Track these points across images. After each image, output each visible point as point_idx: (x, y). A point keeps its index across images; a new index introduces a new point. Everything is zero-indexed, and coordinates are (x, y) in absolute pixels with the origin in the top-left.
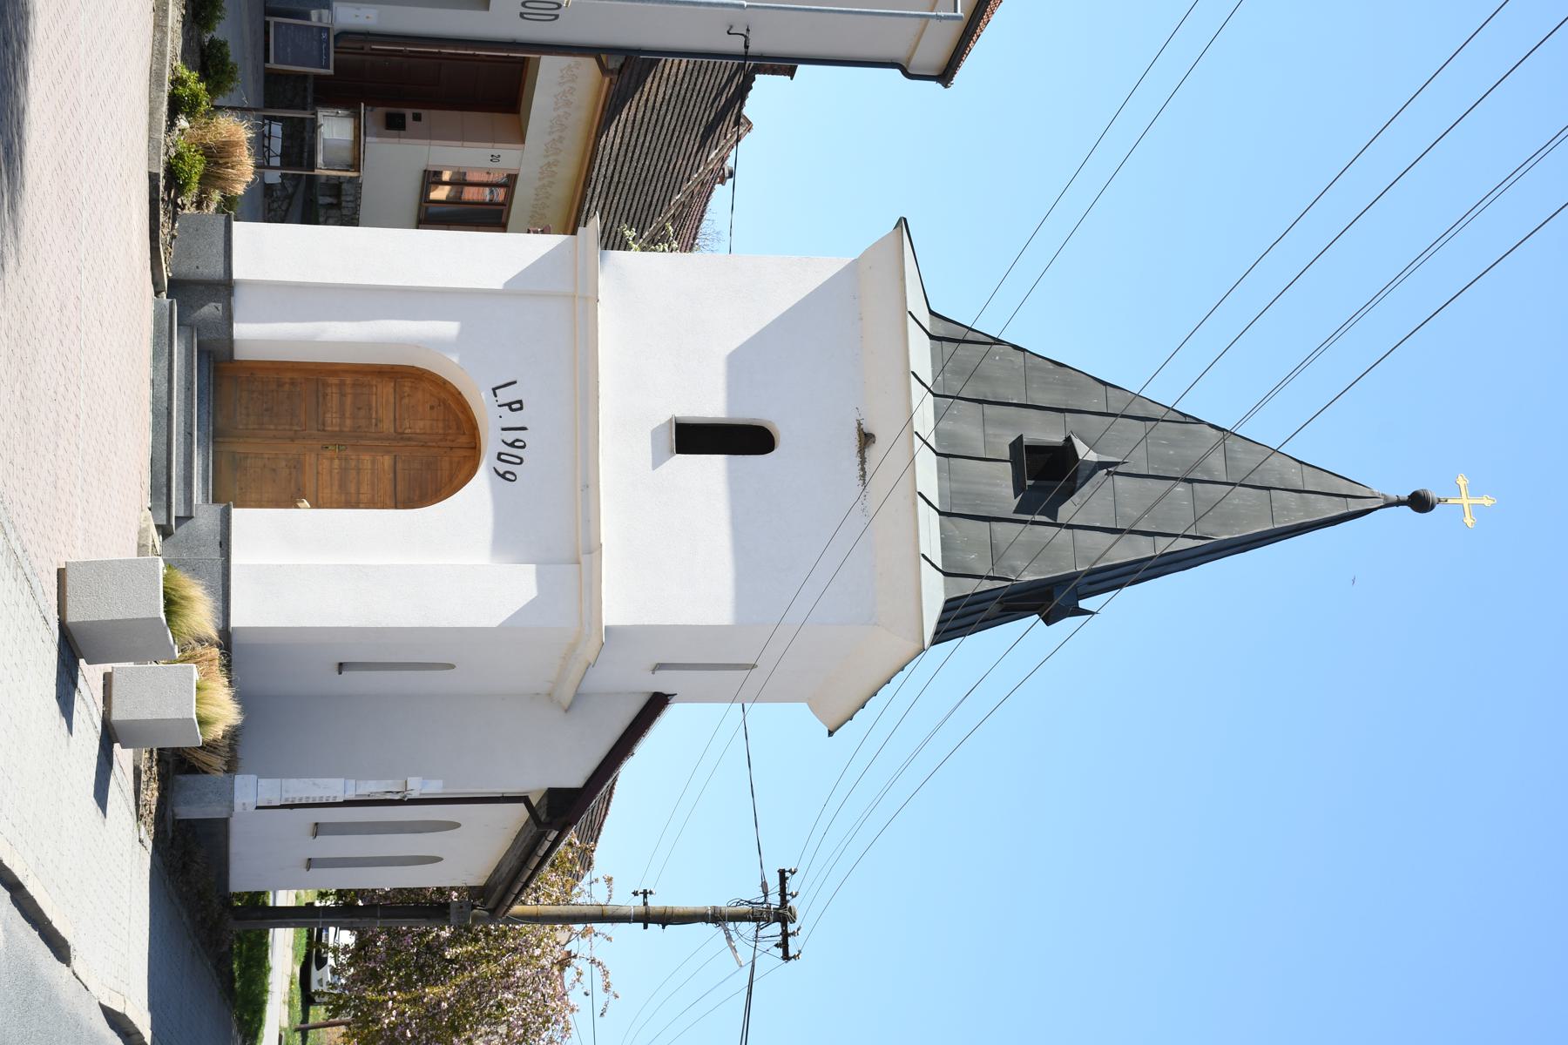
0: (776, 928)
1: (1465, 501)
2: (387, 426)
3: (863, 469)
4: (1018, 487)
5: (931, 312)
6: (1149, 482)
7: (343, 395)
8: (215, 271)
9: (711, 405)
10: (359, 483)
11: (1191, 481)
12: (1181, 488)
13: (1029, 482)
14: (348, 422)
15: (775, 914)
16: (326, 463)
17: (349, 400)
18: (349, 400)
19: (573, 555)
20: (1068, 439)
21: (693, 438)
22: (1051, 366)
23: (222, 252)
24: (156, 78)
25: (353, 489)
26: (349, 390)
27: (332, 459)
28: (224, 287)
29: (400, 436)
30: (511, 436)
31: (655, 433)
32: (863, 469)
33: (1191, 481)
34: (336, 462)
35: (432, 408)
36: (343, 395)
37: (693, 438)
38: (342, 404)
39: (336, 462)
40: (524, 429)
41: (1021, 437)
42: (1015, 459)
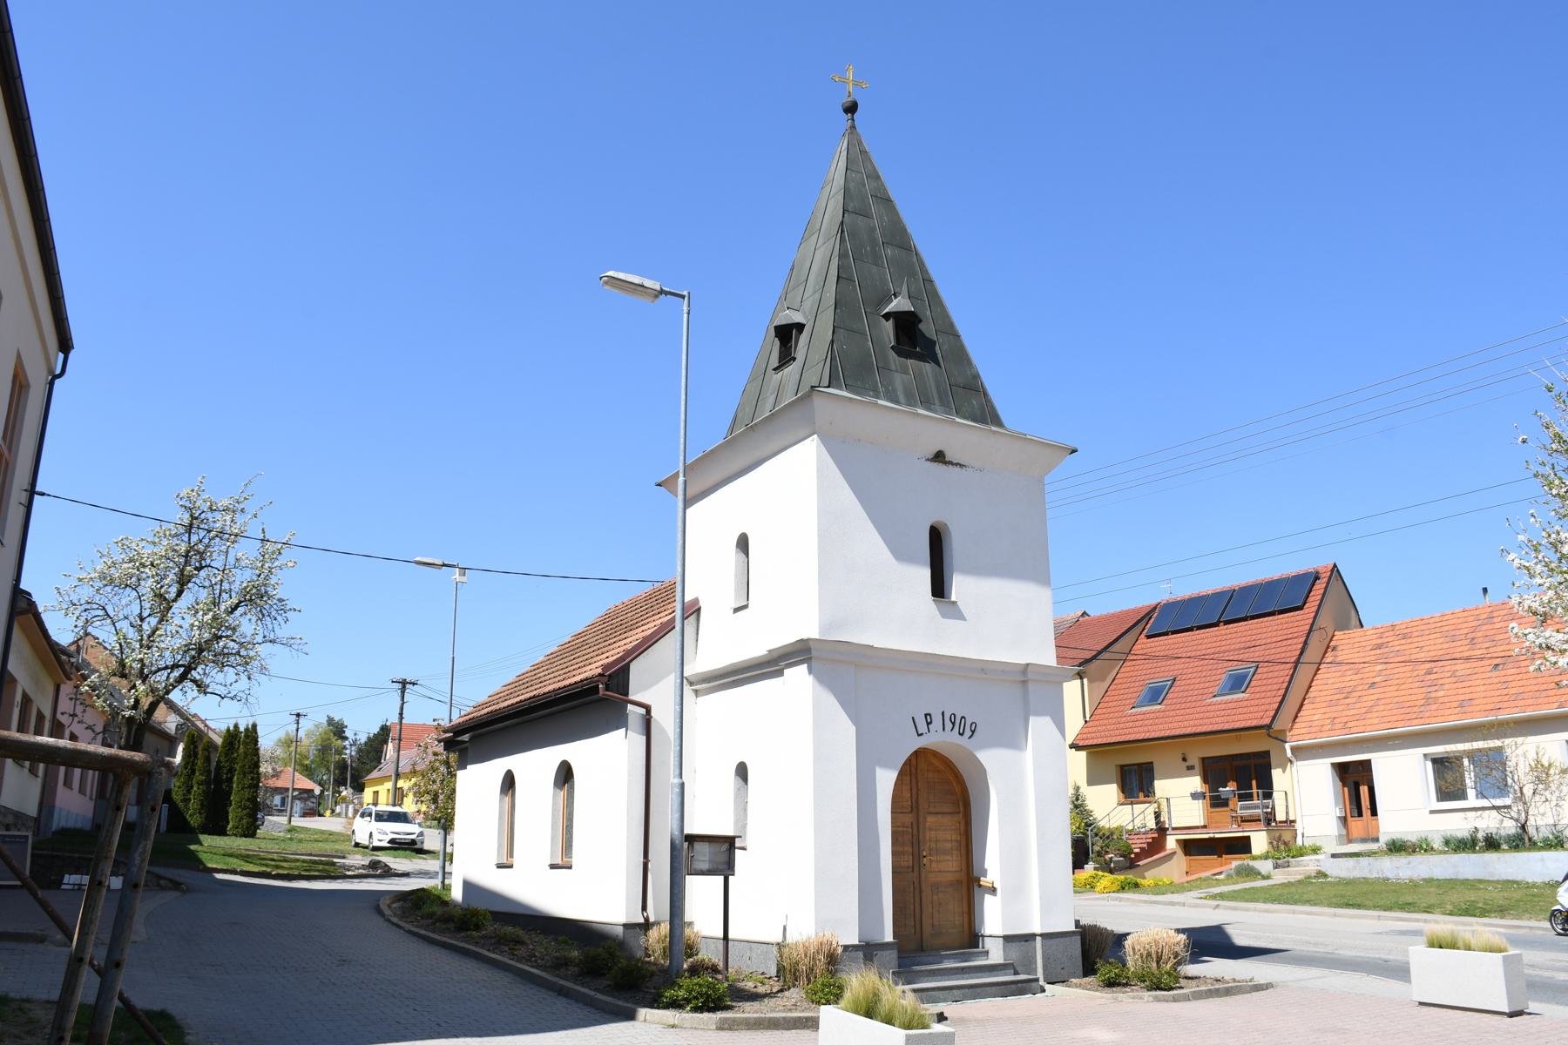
1: (850, 91)
19: (1025, 688)
30: (949, 725)
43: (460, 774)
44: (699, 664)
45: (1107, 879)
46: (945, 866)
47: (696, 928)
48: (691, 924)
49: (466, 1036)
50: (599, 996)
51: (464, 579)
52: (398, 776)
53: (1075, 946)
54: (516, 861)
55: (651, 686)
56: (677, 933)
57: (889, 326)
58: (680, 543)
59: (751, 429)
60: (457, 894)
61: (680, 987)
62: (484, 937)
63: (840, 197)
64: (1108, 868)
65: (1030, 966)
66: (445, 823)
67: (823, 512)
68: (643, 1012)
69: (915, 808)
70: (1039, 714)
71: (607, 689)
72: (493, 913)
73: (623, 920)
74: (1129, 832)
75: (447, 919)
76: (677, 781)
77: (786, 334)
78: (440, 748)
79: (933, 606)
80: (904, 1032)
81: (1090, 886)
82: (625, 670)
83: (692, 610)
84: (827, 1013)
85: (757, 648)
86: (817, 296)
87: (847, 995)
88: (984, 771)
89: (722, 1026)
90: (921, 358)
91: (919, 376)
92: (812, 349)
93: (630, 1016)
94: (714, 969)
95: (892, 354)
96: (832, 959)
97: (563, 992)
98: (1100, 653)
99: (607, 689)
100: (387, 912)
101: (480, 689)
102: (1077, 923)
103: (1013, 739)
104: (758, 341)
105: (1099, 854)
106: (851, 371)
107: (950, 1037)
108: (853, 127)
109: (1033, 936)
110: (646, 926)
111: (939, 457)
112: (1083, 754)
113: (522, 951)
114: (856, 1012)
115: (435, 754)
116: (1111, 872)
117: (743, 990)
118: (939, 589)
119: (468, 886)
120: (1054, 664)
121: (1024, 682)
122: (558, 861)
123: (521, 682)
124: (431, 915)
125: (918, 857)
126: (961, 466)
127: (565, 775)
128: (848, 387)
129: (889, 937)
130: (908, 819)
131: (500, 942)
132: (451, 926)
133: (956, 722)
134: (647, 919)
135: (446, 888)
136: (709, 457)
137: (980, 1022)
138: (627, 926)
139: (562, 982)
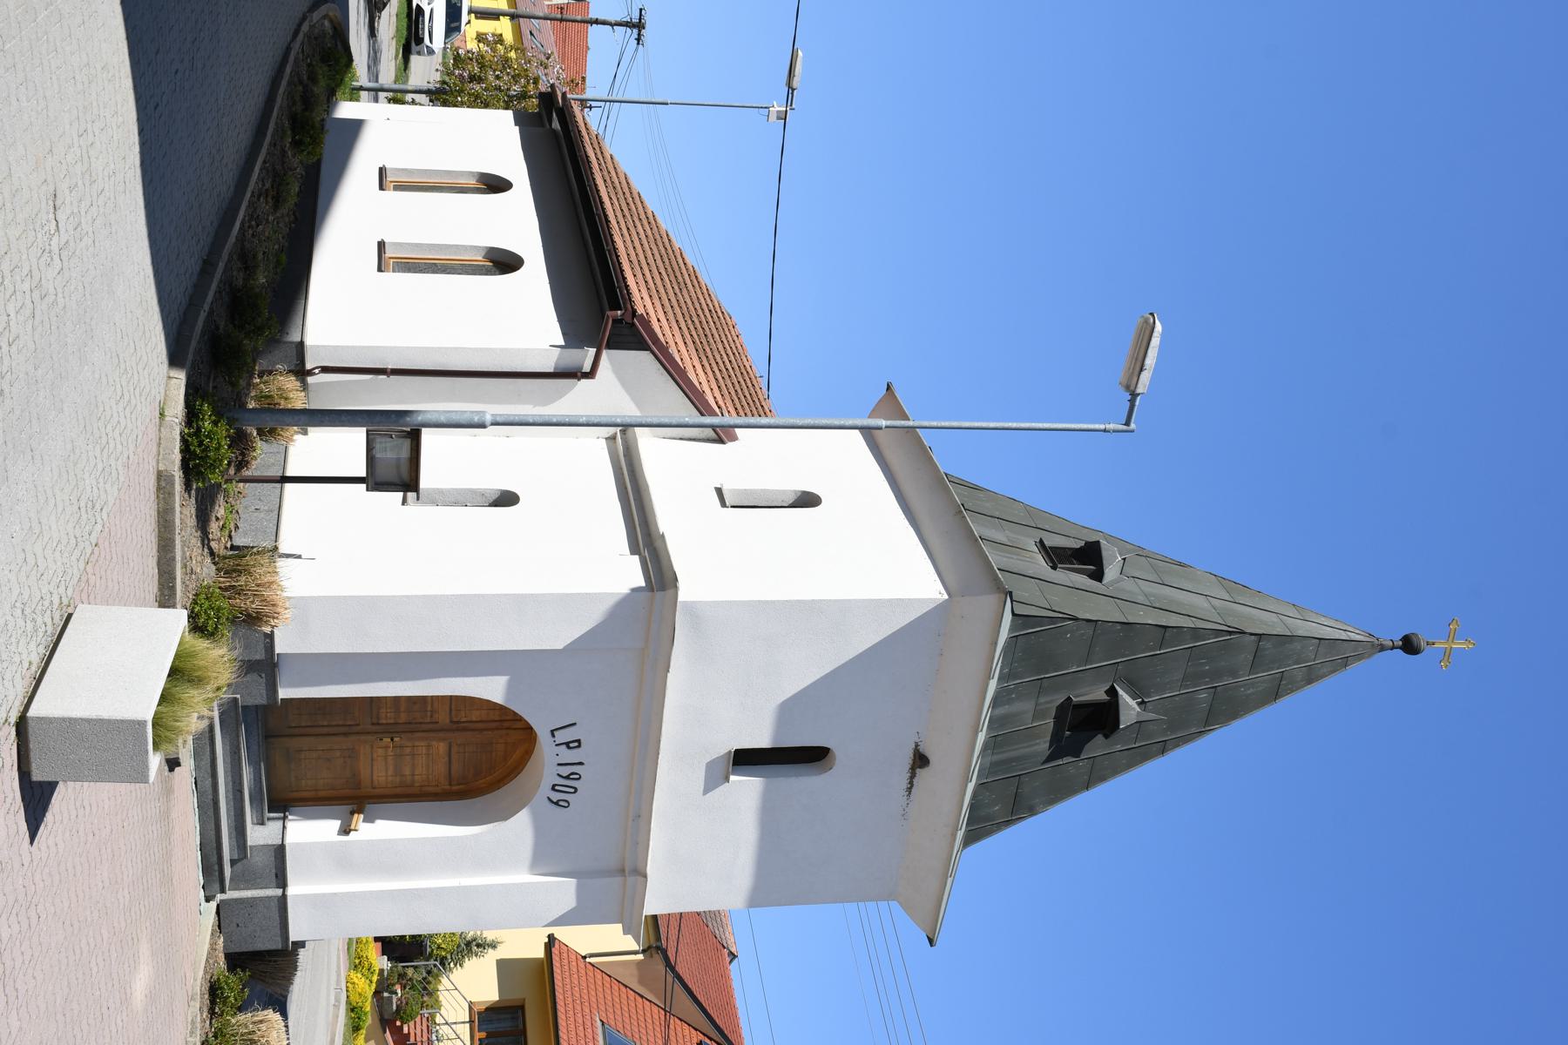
0: (635, 31)
1: (1437, 644)
3: (911, 783)
15: (638, 26)
19: (613, 877)
27: (387, 747)
30: (565, 771)
32: (911, 783)
34: (390, 752)
43: (510, 113)
44: (649, 445)
45: (365, 987)
46: (379, 765)
47: (299, 438)
48: (305, 433)
49: (143, 144)
50: (203, 316)
51: (773, 117)
52: (513, 17)
53: (267, 942)
54: (391, 195)
55: (617, 383)
56: (288, 419)
57: (1098, 694)
58: (799, 422)
59: (959, 511)
60: (346, 110)
61: (215, 423)
62: (284, 152)
63: (1279, 630)
64: (383, 986)
65: (240, 881)
66: (441, 96)
67: (844, 607)
68: (180, 378)
69: (457, 726)
70: (580, 892)
71: (616, 321)
72: (318, 164)
73: (311, 340)
74: (431, 1019)
75: (308, 101)
76: (488, 418)
77: (1088, 557)
78: (543, 88)
79: (723, 751)
80: (149, 717)
81: (358, 964)
82: (640, 345)
83: (721, 435)
84: (178, 619)
85: (667, 520)
86: (1141, 599)
87: (202, 644)
88: (506, 819)
89: (163, 479)
90: (1056, 737)
91: (1030, 734)
92: (1068, 593)
93: (175, 360)
94: (242, 464)
95: (1060, 699)
96: (253, 619)
97: (207, 266)
98: (673, 969)
99: (616, 321)
100: (316, 16)
101: (622, 142)
102: (301, 944)
103: (545, 858)
104: (1083, 515)
105: (402, 976)
106: (1036, 644)
107: (142, 777)
108: (1382, 648)
109: (282, 883)
110: (301, 373)
111: (920, 760)
112: (540, 953)
113: (264, 206)
114: (177, 656)
115: (536, 81)
116: (377, 993)
117: (213, 503)
118: (745, 759)
119: (355, 126)
120: (650, 909)
121: (622, 871)
122: (389, 253)
123: (632, 199)
124: (313, 78)
125: (391, 730)
126: (909, 790)
127: (504, 262)
128: (1013, 641)
129: (283, 693)
130: (443, 717)
131: (277, 176)
132: (299, 107)
133: (569, 781)
134: (311, 373)
135: (354, 95)
136: (923, 453)
137: (166, 816)
138: (301, 345)
139: (221, 265)
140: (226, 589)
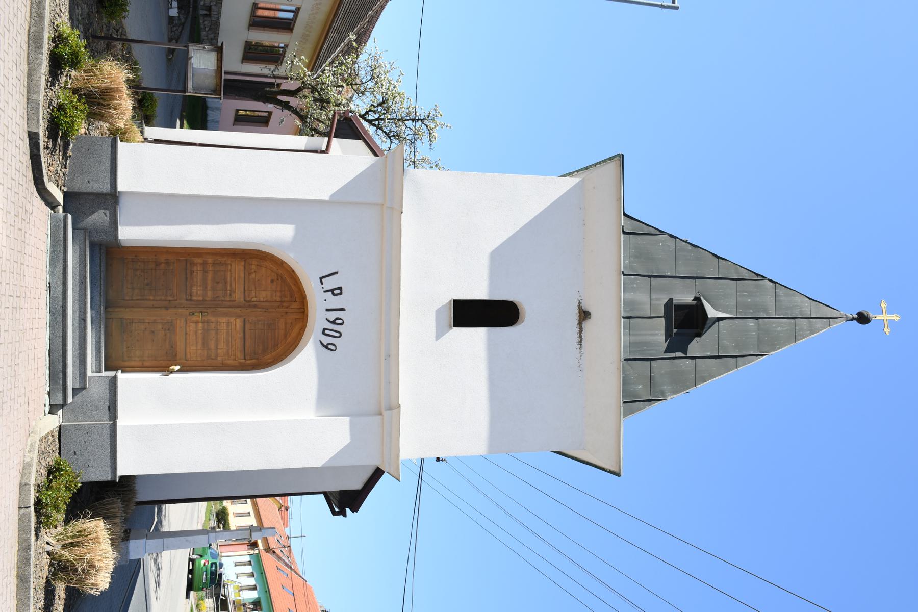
1: (884, 317)
2: (239, 296)
3: (580, 337)
4: (668, 334)
5: (625, 215)
6: (737, 321)
7: (205, 272)
8: (106, 188)
9: (478, 290)
10: (217, 341)
11: (757, 318)
12: (752, 323)
13: (675, 331)
14: (210, 293)
16: (192, 325)
17: (210, 276)
18: (210, 276)
20: (697, 299)
21: (467, 313)
22: (690, 247)
23: (109, 168)
24: (34, 40)
25: (212, 346)
26: (210, 268)
27: (197, 322)
28: (111, 199)
29: (249, 304)
30: (332, 316)
31: (438, 312)
32: (580, 337)
33: (757, 318)
34: (200, 325)
35: (272, 281)
36: (205, 272)
37: (467, 313)
38: (204, 280)
39: (200, 325)
40: (343, 309)
41: (671, 300)
42: (667, 316)
70: (352, 426)
140: (80, 536)
